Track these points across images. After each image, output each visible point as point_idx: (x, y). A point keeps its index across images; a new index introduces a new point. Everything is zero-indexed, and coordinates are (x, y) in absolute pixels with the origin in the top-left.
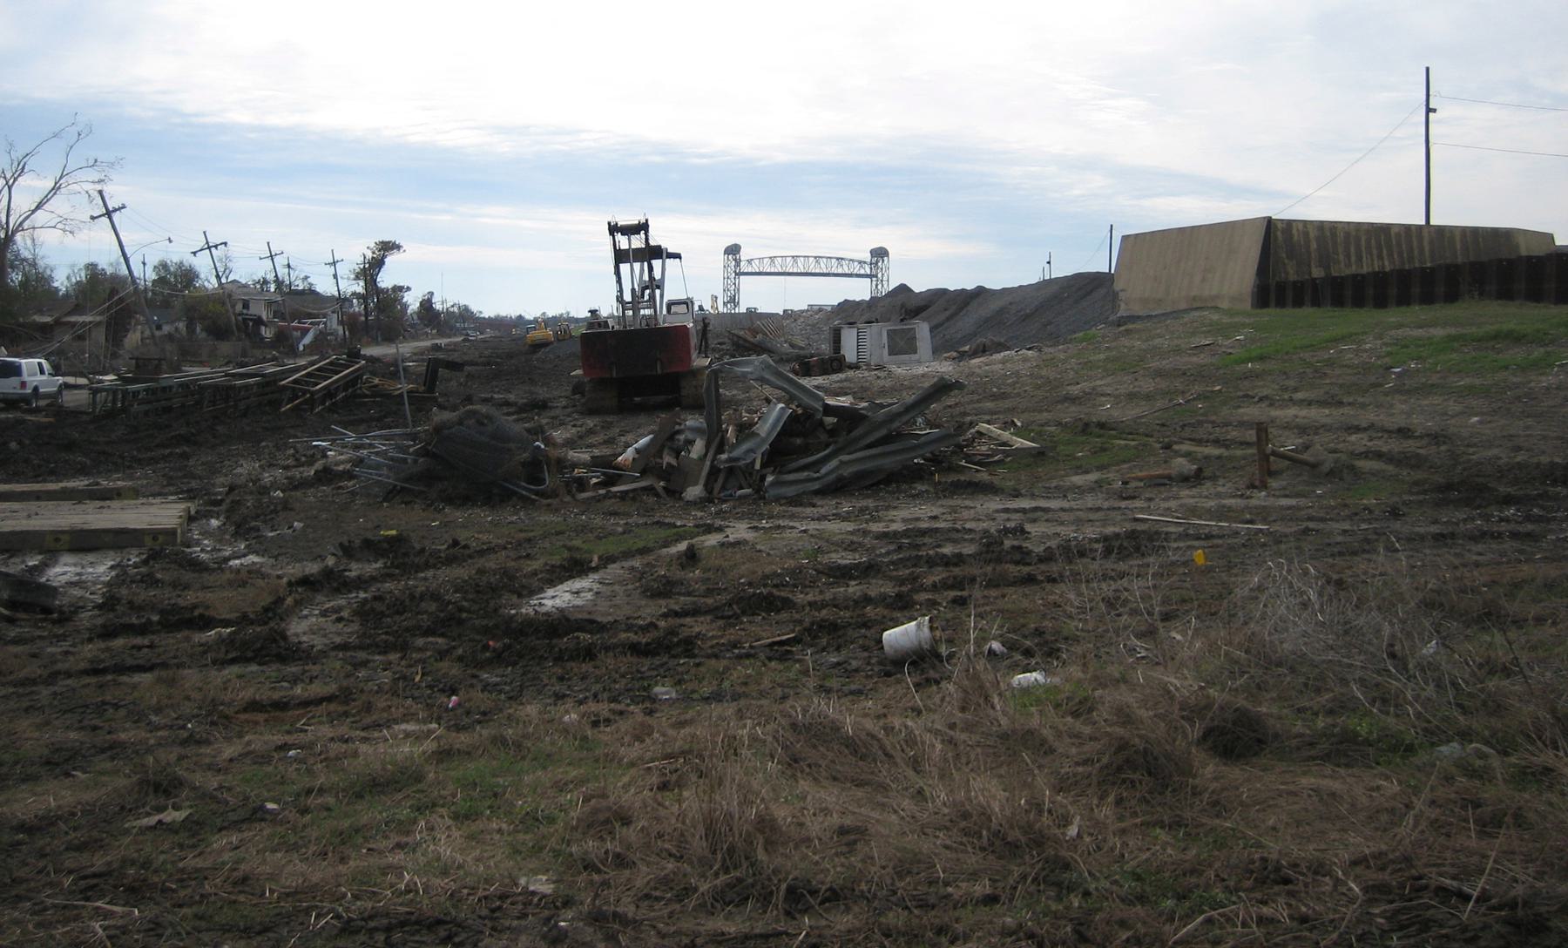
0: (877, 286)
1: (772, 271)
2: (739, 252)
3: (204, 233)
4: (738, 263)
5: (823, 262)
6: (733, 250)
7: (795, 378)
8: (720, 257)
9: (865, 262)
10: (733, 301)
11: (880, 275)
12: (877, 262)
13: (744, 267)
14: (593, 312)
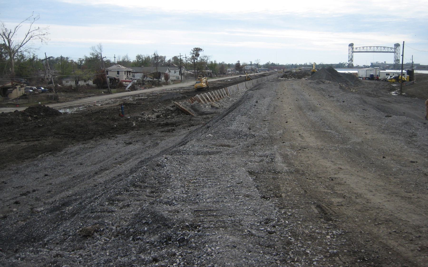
0: (396, 55)
1: (356, 51)
2: (353, 46)
3: (45, 53)
4: (353, 48)
5: (372, 48)
6: (351, 45)
8: (347, 47)
9: (392, 48)
11: (397, 52)
13: (355, 50)
14: (385, 62)
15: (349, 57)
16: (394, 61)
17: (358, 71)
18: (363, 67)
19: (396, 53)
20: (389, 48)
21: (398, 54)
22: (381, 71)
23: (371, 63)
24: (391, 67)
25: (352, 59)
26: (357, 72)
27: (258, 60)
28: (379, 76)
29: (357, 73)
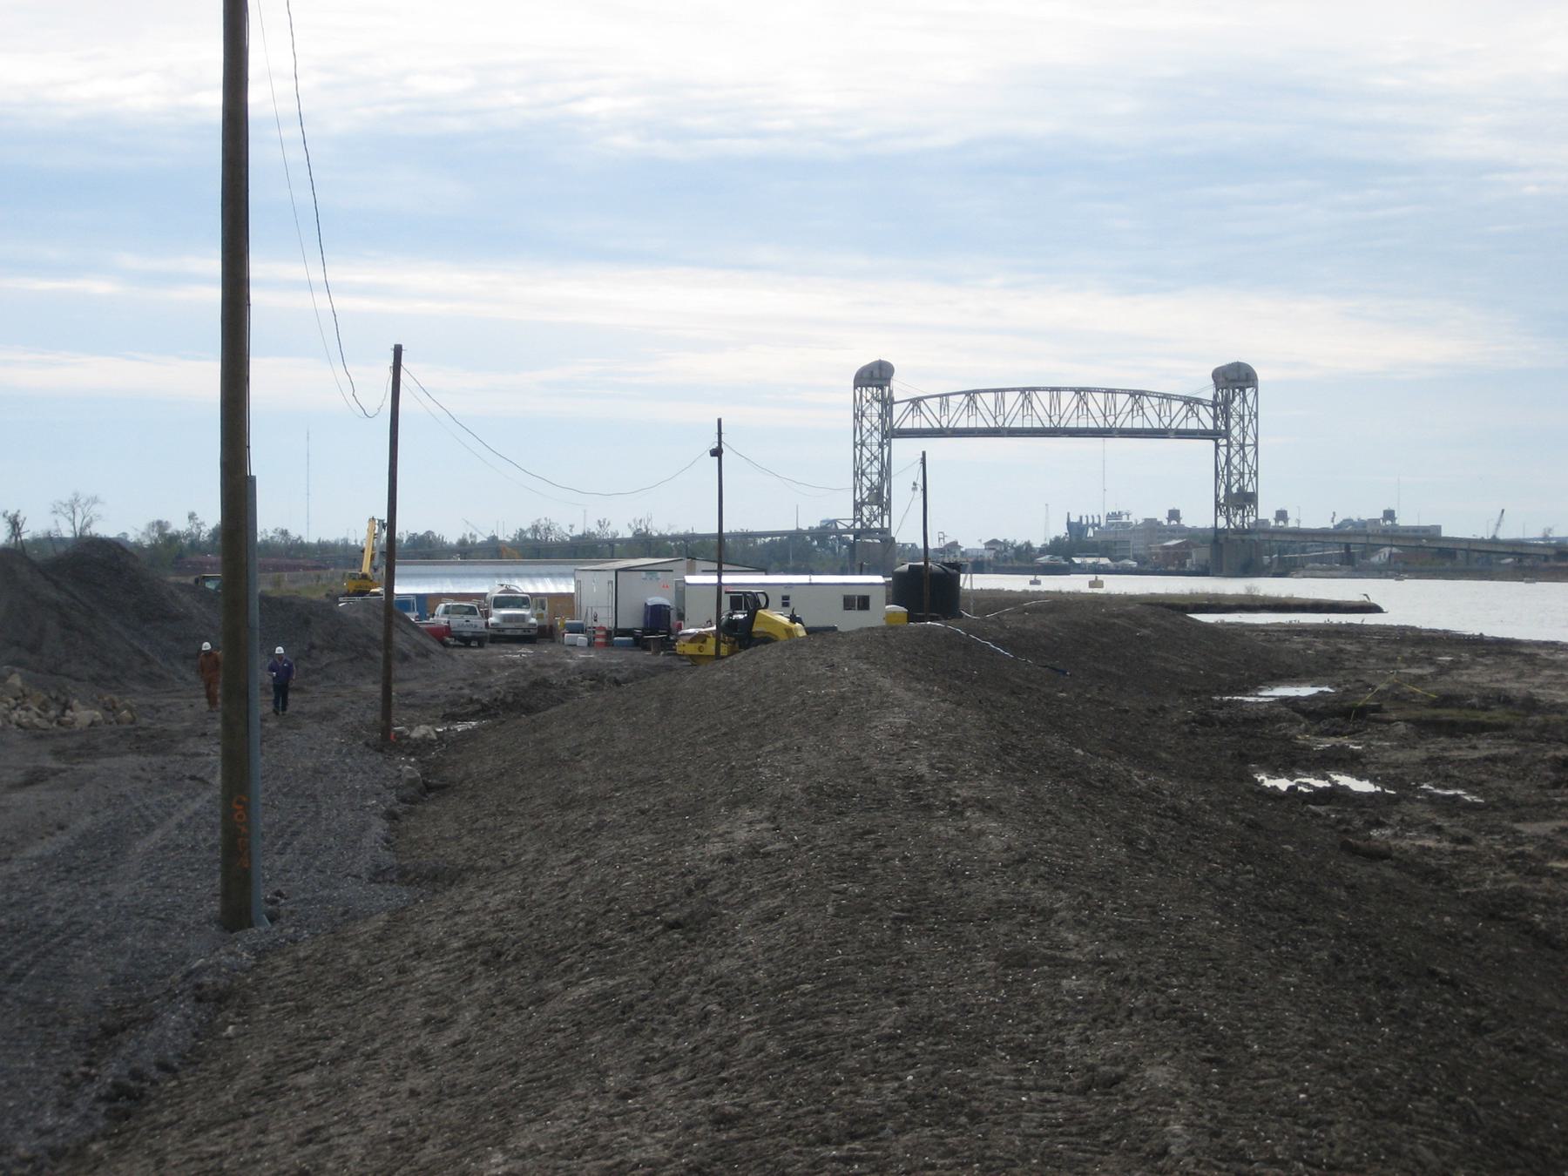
4: (887, 403)
5: (1096, 402)
6: (875, 376)
7: (1321, 689)
8: (844, 394)
9: (1198, 401)
10: (1246, 499)
11: (1236, 432)
12: (1227, 402)
13: (902, 417)
14: (1174, 515)
15: (859, 473)
16: (1217, 505)
17: (578, 584)
18: (989, 555)
19: (1229, 446)
20: (1177, 405)
21: (1242, 446)
22: (690, 579)
23: (1070, 525)
24: (1198, 556)
25: (880, 489)
26: (572, 589)
27: (76, 500)
28: (681, 616)
29: (570, 596)
